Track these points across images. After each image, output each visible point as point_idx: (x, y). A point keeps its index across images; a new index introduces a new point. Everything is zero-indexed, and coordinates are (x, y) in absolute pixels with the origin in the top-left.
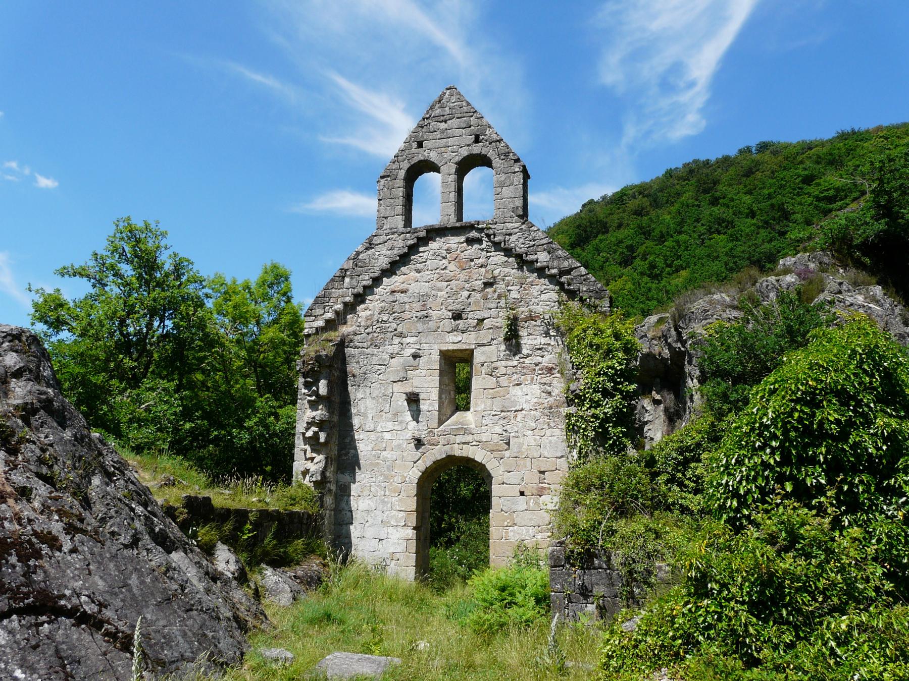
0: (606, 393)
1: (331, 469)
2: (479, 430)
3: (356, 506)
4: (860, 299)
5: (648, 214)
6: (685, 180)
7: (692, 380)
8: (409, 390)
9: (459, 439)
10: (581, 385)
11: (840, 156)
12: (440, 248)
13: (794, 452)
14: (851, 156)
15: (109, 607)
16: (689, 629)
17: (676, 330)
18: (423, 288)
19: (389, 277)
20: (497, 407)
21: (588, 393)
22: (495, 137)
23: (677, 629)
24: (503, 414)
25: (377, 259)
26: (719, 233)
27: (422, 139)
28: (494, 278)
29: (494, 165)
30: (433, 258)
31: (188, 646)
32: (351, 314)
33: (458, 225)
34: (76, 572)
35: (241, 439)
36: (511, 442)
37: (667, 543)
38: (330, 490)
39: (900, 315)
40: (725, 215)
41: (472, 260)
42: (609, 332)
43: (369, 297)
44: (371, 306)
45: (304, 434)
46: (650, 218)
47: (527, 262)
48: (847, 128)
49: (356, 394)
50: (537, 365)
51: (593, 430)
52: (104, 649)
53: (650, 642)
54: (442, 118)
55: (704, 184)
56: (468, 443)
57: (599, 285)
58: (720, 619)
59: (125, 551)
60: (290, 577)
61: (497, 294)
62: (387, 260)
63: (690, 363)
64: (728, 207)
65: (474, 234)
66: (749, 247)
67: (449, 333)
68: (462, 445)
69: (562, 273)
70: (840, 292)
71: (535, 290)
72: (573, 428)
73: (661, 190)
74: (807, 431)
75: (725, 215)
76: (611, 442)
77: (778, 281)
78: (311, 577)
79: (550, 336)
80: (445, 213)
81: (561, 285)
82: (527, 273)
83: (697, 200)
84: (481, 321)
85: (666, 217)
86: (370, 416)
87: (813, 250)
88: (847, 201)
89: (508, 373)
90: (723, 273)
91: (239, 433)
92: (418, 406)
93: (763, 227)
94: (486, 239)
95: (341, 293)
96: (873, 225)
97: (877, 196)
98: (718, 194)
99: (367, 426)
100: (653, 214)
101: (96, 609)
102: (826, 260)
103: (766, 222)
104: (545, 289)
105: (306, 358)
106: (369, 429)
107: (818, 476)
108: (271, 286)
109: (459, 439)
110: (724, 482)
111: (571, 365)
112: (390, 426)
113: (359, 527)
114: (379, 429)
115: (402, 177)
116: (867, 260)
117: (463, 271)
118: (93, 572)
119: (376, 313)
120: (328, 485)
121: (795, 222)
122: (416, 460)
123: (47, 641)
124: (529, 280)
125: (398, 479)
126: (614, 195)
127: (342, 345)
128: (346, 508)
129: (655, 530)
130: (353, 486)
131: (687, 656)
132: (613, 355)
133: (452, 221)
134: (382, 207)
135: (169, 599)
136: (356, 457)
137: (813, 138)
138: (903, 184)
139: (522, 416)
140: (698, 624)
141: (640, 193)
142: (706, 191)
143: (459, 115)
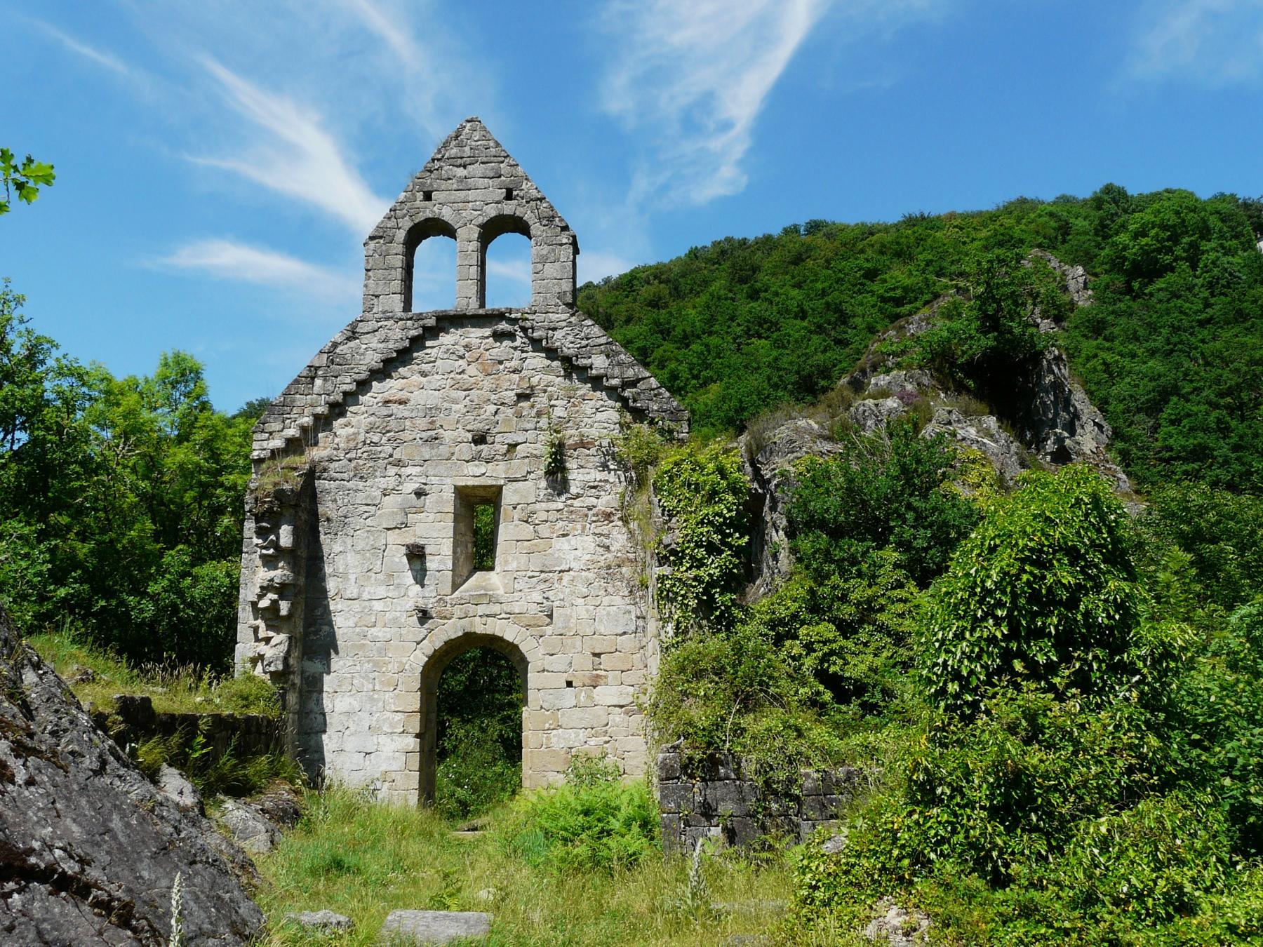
0: (712, 549)
1: (295, 654)
2: (510, 597)
3: (331, 706)
4: (972, 432)
5: (666, 306)
6: (714, 264)
7: (777, 531)
8: (410, 541)
9: (481, 610)
10: (678, 537)
11: (908, 247)
12: (456, 344)
13: (1024, 623)
14: (920, 248)
15: (93, 864)
16: (918, 845)
17: (753, 464)
18: (432, 398)
19: (381, 380)
20: (535, 564)
21: (688, 548)
22: (534, 193)
23: (903, 847)
24: (543, 575)
25: (363, 354)
26: (760, 337)
27: (430, 189)
28: (532, 388)
29: (533, 232)
30: (446, 356)
31: (205, 915)
32: (324, 431)
33: (481, 312)
34: (40, 814)
35: (142, 611)
36: (555, 615)
37: (813, 744)
38: (294, 684)
39: (1017, 454)
40: (768, 313)
41: (501, 362)
42: (711, 466)
43: (351, 409)
44: (354, 421)
45: (254, 604)
46: (670, 313)
47: (578, 367)
48: (915, 211)
49: (331, 545)
50: (590, 509)
51: (695, 598)
52: (97, 927)
53: (866, 865)
54: (459, 161)
55: (741, 270)
56: (494, 616)
57: (675, 404)
58: (954, 832)
59: (96, 780)
60: (257, 811)
61: (535, 410)
62: (378, 357)
63: (773, 508)
64: (771, 303)
65: (503, 326)
66: (799, 357)
67: (467, 462)
68: (485, 618)
69: (627, 384)
70: (950, 423)
71: (588, 407)
72: (668, 595)
73: (683, 276)
74: (1034, 597)
75: (768, 313)
76: (718, 613)
77: (877, 405)
78: (284, 810)
79: (610, 471)
80: (464, 295)
81: (624, 401)
82: (577, 384)
83: (731, 291)
84: (513, 447)
85: (691, 313)
86: (352, 577)
87: (909, 367)
88: (918, 304)
89: (550, 519)
90: (765, 389)
91: (139, 603)
92: (423, 563)
93: (816, 333)
94: (521, 334)
95: (309, 401)
96: (979, 339)
97: (983, 304)
98: (758, 285)
99: (348, 592)
100: (673, 307)
101: (77, 868)
102: (925, 381)
103: (819, 326)
104: (602, 406)
105: (260, 494)
106: (350, 596)
107: (1049, 651)
108: (174, 384)
109: (481, 610)
110: (940, 661)
111: (660, 511)
112: (382, 591)
113: (335, 736)
114: (365, 596)
115: (402, 240)
116: (971, 382)
117: (488, 377)
118: (62, 813)
119: (361, 431)
120: (292, 677)
121: (855, 328)
122: (419, 639)
123: (23, 919)
124: (580, 393)
125: (394, 667)
126: (621, 277)
127: (311, 475)
128: (316, 709)
129: (796, 726)
130: (326, 678)
131: (916, 879)
132: (720, 499)
133: (473, 307)
134: (371, 281)
135: (165, 848)
136: (332, 637)
137: (875, 221)
138: (1014, 291)
139: (569, 578)
140: (928, 838)
141: (656, 277)
142: (743, 281)
143: (485, 159)
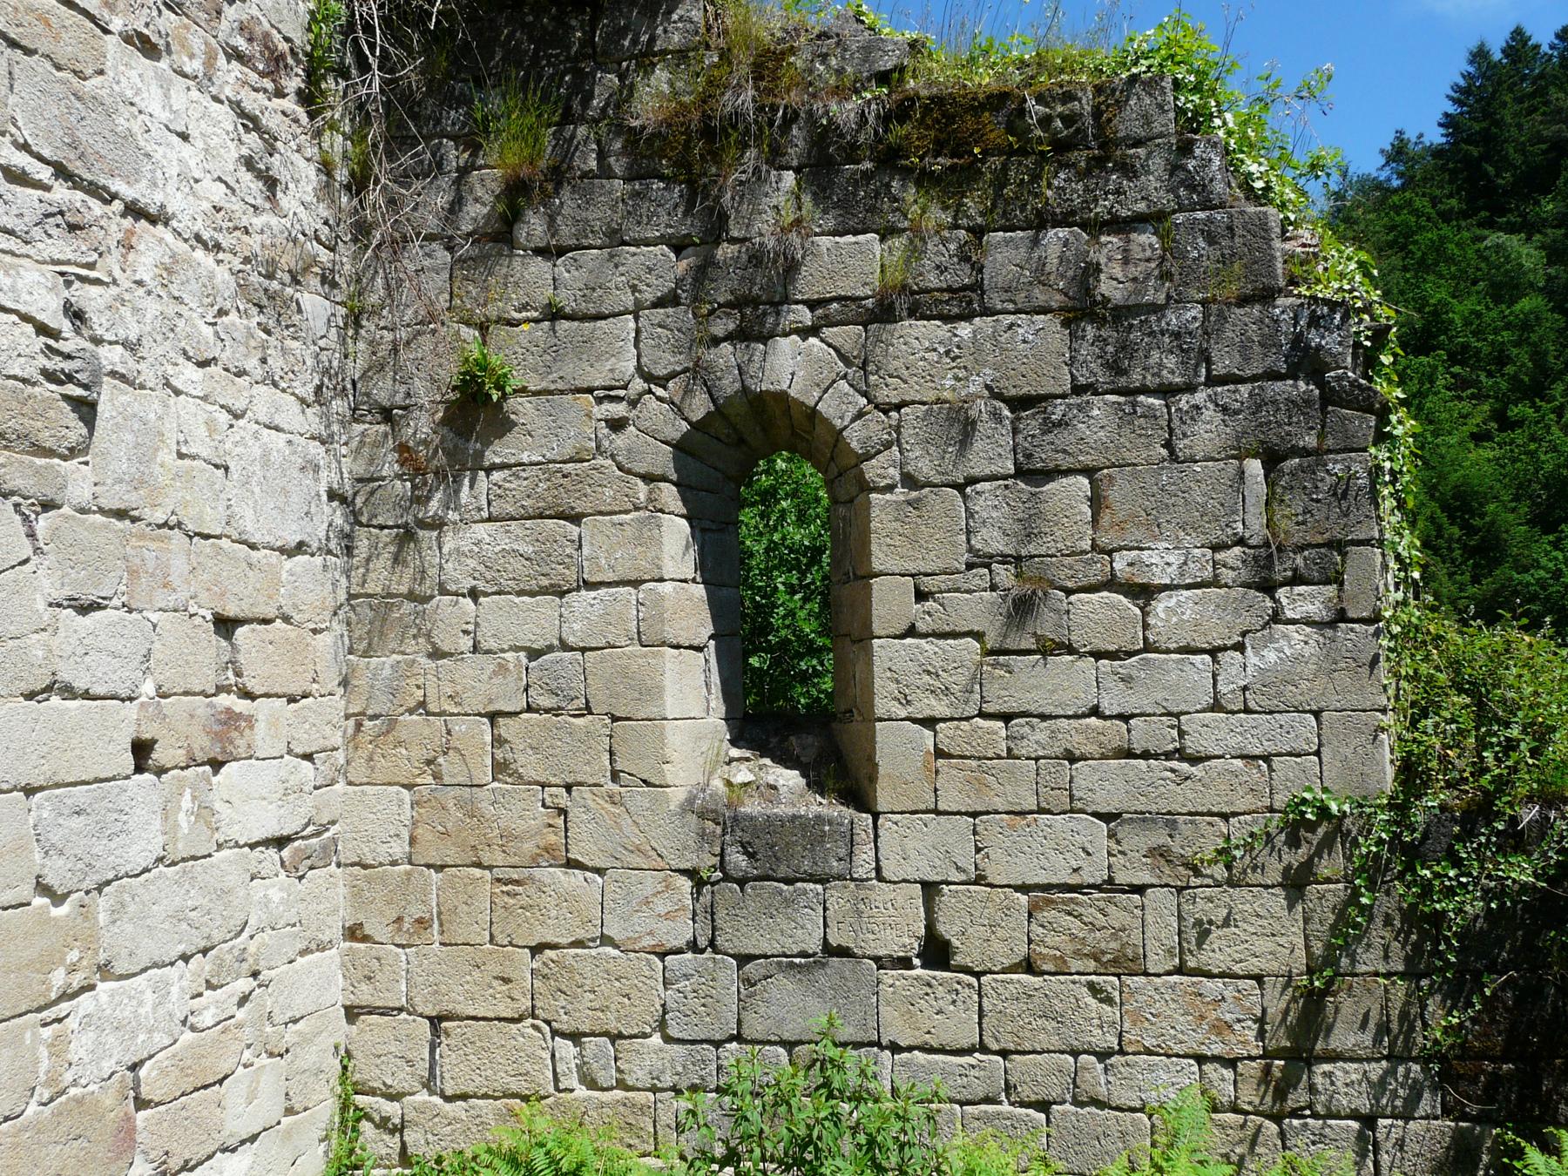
24: (61, 193)
